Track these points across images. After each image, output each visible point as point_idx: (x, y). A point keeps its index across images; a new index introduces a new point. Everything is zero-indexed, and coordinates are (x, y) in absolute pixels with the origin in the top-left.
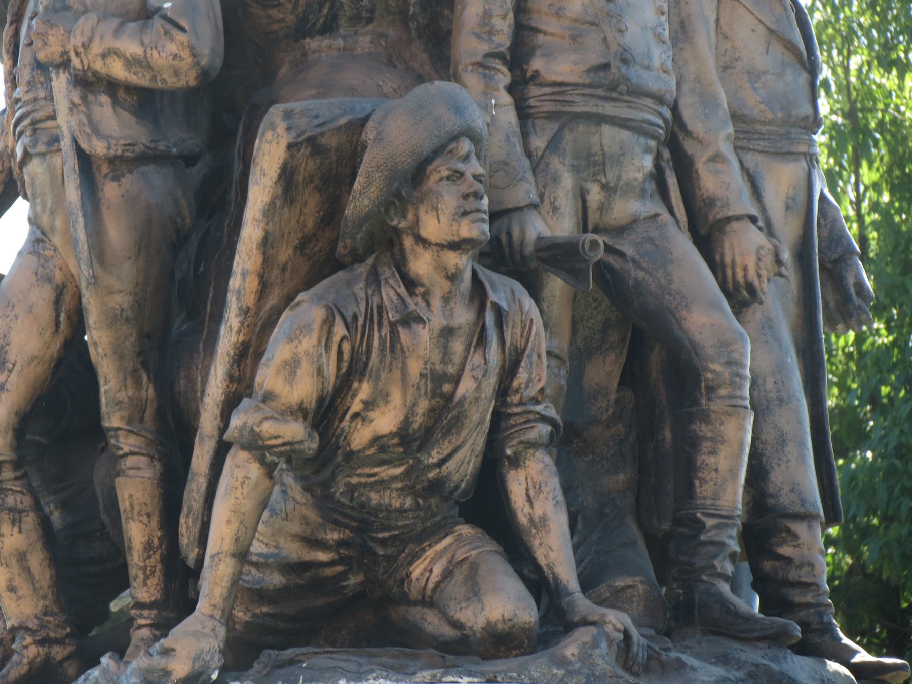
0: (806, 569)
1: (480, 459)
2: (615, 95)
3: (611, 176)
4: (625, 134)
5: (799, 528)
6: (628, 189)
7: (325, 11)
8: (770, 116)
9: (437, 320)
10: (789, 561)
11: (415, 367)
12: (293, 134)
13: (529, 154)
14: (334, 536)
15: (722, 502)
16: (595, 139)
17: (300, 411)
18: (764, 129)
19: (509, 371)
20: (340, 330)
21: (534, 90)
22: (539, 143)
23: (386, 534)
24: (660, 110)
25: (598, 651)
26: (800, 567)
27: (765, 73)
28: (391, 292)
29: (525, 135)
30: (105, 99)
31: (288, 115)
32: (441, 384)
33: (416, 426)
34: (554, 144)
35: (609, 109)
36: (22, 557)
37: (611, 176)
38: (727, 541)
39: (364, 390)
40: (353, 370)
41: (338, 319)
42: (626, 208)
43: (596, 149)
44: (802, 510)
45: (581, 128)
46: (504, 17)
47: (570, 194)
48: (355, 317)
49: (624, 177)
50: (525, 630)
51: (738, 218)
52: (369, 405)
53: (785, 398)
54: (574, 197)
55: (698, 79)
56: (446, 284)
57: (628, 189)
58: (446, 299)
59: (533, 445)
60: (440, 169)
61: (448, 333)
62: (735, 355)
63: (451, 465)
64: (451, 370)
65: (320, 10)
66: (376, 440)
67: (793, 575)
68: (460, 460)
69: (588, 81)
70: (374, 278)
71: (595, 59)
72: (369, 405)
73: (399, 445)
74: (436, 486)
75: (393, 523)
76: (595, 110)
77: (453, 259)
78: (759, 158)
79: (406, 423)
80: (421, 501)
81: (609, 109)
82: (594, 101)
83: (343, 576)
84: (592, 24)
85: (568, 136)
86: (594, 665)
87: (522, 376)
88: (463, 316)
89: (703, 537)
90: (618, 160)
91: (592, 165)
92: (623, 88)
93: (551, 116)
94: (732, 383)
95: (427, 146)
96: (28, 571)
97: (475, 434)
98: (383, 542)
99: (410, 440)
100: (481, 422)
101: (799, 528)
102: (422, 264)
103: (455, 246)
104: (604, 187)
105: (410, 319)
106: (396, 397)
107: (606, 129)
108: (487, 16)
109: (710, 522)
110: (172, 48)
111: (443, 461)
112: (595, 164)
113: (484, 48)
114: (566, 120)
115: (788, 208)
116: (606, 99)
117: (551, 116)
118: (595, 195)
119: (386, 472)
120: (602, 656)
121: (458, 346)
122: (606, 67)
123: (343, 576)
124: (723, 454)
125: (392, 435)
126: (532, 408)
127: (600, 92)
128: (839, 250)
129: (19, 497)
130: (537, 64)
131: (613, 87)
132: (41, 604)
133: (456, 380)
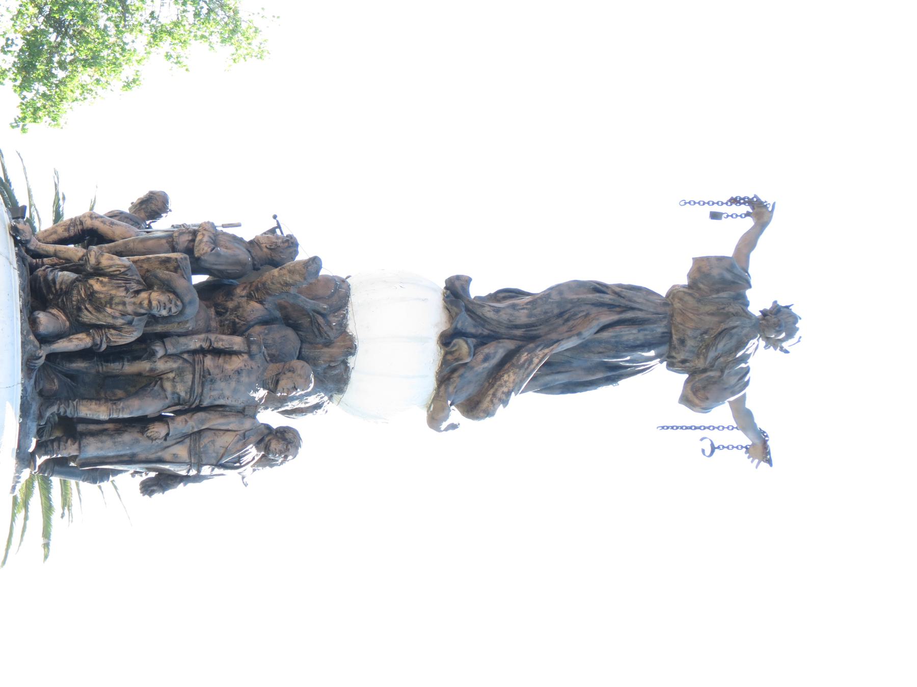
3: (177, 379)
5: (76, 446)
6: (174, 387)
9: (127, 300)
10: (66, 442)
11: (113, 292)
13: (183, 353)
14: (64, 287)
17: (99, 263)
19: (114, 327)
20: (123, 270)
21: (201, 356)
22: (185, 356)
24: (196, 386)
28: (135, 287)
29: (188, 352)
30: (190, 238)
31: (186, 258)
32: (110, 301)
34: (185, 360)
35: (197, 376)
36: (55, 232)
37: (177, 379)
39: (105, 280)
40: (112, 276)
42: (168, 385)
45: (191, 369)
50: (37, 328)
52: (101, 282)
57: (174, 387)
58: (134, 303)
59: (94, 338)
60: (172, 296)
61: (124, 304)
63: (86, 312)
66: (92, 286)
67: (62, 443)
68: (88, 317)
70: (138, 282)
72: (101, 282)
74: (79, 309)
77: (146, 303)
78: (188, 444)
79: (97, 292)
81: (197, 376)
83: (52, 293)
85: (188, 365)
87: (113, 332)
88: (130, 309)
90: (182, 381)
91: (180, 372)
93: (194, 360)
95: (178, 291)
96: (51, 234)
98: (63, 300)
99: (92, 296)
100: (99, 320)
101: (76, 446)
102: (144, 295)
103: (150, 302)
105: (127, 290)
106: (104, 289)
107: (191, 376)
108: (223, 340)
110: (206, 248)
111: (86, 309)
113: (213, 339)
114: (193, 365)
117: (194, 360)
118: (171, 375)
119: (82, 293)
121: (120, 307)
123: (52, 293)
130: (209, 357)
131: (204, 377)
133: (111, 308)
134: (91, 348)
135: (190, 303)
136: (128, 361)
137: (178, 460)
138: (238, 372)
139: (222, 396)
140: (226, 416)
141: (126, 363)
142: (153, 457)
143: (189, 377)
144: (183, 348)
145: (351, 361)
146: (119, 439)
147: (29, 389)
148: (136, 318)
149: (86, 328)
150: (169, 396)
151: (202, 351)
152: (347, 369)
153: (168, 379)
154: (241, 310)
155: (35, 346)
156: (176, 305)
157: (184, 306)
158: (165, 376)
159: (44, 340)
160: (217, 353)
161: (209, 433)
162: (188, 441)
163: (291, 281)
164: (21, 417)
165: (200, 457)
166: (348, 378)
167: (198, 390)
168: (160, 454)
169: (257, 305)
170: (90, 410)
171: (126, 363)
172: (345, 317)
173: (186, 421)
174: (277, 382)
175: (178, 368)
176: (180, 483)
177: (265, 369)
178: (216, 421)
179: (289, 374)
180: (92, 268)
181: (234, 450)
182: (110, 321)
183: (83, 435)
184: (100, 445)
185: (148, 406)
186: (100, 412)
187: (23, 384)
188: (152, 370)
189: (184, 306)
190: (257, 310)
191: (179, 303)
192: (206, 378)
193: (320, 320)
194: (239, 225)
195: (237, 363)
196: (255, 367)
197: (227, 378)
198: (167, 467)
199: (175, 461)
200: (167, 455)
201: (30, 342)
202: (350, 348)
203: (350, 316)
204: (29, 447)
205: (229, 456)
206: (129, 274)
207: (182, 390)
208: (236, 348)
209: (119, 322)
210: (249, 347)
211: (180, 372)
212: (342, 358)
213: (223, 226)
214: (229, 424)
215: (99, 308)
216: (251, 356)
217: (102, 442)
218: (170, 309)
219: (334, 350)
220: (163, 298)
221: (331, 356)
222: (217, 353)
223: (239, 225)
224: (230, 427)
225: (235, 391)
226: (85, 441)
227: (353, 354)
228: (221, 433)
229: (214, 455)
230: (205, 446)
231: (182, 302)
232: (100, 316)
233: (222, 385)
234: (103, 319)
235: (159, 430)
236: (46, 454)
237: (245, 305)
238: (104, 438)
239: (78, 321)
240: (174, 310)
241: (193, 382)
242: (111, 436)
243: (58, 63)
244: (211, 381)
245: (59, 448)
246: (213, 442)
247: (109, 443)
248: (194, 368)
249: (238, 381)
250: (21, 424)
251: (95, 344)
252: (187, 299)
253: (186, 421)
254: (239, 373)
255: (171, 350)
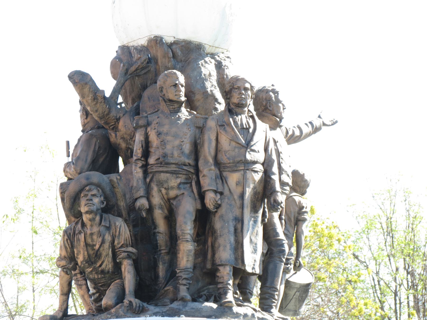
0: (222, 278)
1: (112, 263)
2: (162, 165)
3: (165, 185)
4: (168, 175)
6: (172, 188)
7: (129, 152)
8: (229, 162)
9: (89, 232)
12: (62, 190)
15: (181, 266)
16: (160, 177)
18: (229, 165)
22: (148, 180)
23: (100, 284)
24: (169, 169)
25: (120, 310)
26: (220, 278)
27: (229, 151)
29: (145, 178)
33: (86, 258)
34: (151, 180)
37: (165, 185)
38: (182, 275)
41: (66, 235)
42: (172, 193)
43: (161, 179)
44: (220, 263)
46: (139, 149)
47: (157, 192)
48: (70, 234)
49: (170, 185)
51: (208, 190)
52: (77, 254)
53: (222, 234)
54: (159, 192)
55: (204, 156)
56: (90, 222)
58: (92, 226)
61: (92, 234)
62: (183, 228)
63: (103, 266)
64: (94, 243)
65: (128, 152)
68: (107, 264)
69: (156, 163)
71: (157, 157)
72: (77, 254)
73: (86, 263)
74: (103, 272)
75: (100, 282)
76: (158, 170)
78: (227, 173)
79: (84, 258)
80: (103, 276)
81: (161, 169)
82: (158, 168)
84: (158, 148)
85: (155, 177)
86: (119, 313)
87: (116, 242)
88: (95, 229)
89: (177, 275)
90: (166, 181)
91: (160, 184)
92: (163, 163)
94: (182, 235)
97: (107, 258)
98: (101, 286)
100: (107, 255)
101: (221, 268)
104: (165, 189)
107: (162, 174)
108: (136, 150)
109: (178, 271)
111: (100, 266)
112: (161, 183)
115: (237, 184)
116: (161, 167)
118: (164, 191)
120: (122, 311)
121: (95, 237)
122: (159, 159)
124: (180, 253)
125: (83, 261)
126: (120, 249)
127: (159, 165)
128: (271, 192)
129: (82, 282)
131: (161, 163)
132: (88, 307)
133: (95, 245)
134: (134, 260)
135: (88, 179)
136: (155, 228)
137: (242, 180)
138: (159, 134)
139: (180, 148)
140: (203, 142)
141: (157, 230)
142: (238, 202)
143: (163, 176)
144: (141, 183)
145: (169, 39)
146: (218, 232)
147: (157, 310)
148: (103, 223)
149: (117, 266)
150: (182, 192)
151: (145, 167)
152: (176, 43)
153: (167, 194)
154: (125, 136)
155: (121, 307)
156: (90, 190)
157: (91, 184)
158: (166, 197)
159: (120, 297)
160: (146, 154)
161: (220, 156)
162: (225, 174)
163: (91, 95)
164: (179, 316)
165: (238, 162)
166: (184, 41)
167: (173, 168)
168: (236, 197)
169: (121, 123)
170: (183, 258)
171: (157, 230)
172: (136, 48)
173: (204, 176)
174: (171, 101)
175: (157, 185)
176: (271, 178)
177: (162, 112)
178: (208, 150)
179: (164, 91)
180: (70, 263)
181: (233, 133)
182: (107, 245)
183: (213, 263)
184: (221, 248)
185: (187, 209)
186: (187, 249)
187: (151, 316)
188: (161, 208)
189: (91, 184)
190: (125, 123)
191: (87, 188)
192: (163, 161)
193: (133, 69)
194: (68, 143)
195: (153, 137)
196: (157, 120)
197: (163, 143)
198: (249, 192)
199: (242, 183)
200: (237, 191)
201: (116, 312)
202: (157, 41)
203: (135, 44)
204: (212, 308)
205: (237, 137)
206: (69, 231)
207: (174, 182)
208: (142, 138)
209: (108, 238)
210: (141, 127)
211: (160, 184)
212: (166, 48)
213: (68, 156)
214: (210, 140)
215: (98, 255)
216: (148, 124)
217: (219, 246)
218: (94, 195)
219: (159, 55)
220: (83, 202)
221: (164, 57)
222: (146, 154)
223: (68, 143)
224: (213, 138)
225: (176, 136)
226: (218, 262)
227: (161, 39)
228: (219, 145)
229: (237, 150)
230: (229, 158)
231: (87, 186)
232: (104, 254)
233: (169, 147)
234: (106, 251)
235: (210, 199)
236: (226, 293)
237: (121, 133)
238: (216, 245)
239: (113, 273)
240: (95, 192)
241: (167, 172)
242: (216, 239)
243: (362, 317)
244: (164, 157)
245: (222, 283)
246: (226, 152)
247: (221, 241)
248: (156, 172)
249: (167, 134)
250: (187, 315)
251: (129, 257)
252: (84, 182)
253: (204, 176)
254: (160, 134)
255: (142, 192)
